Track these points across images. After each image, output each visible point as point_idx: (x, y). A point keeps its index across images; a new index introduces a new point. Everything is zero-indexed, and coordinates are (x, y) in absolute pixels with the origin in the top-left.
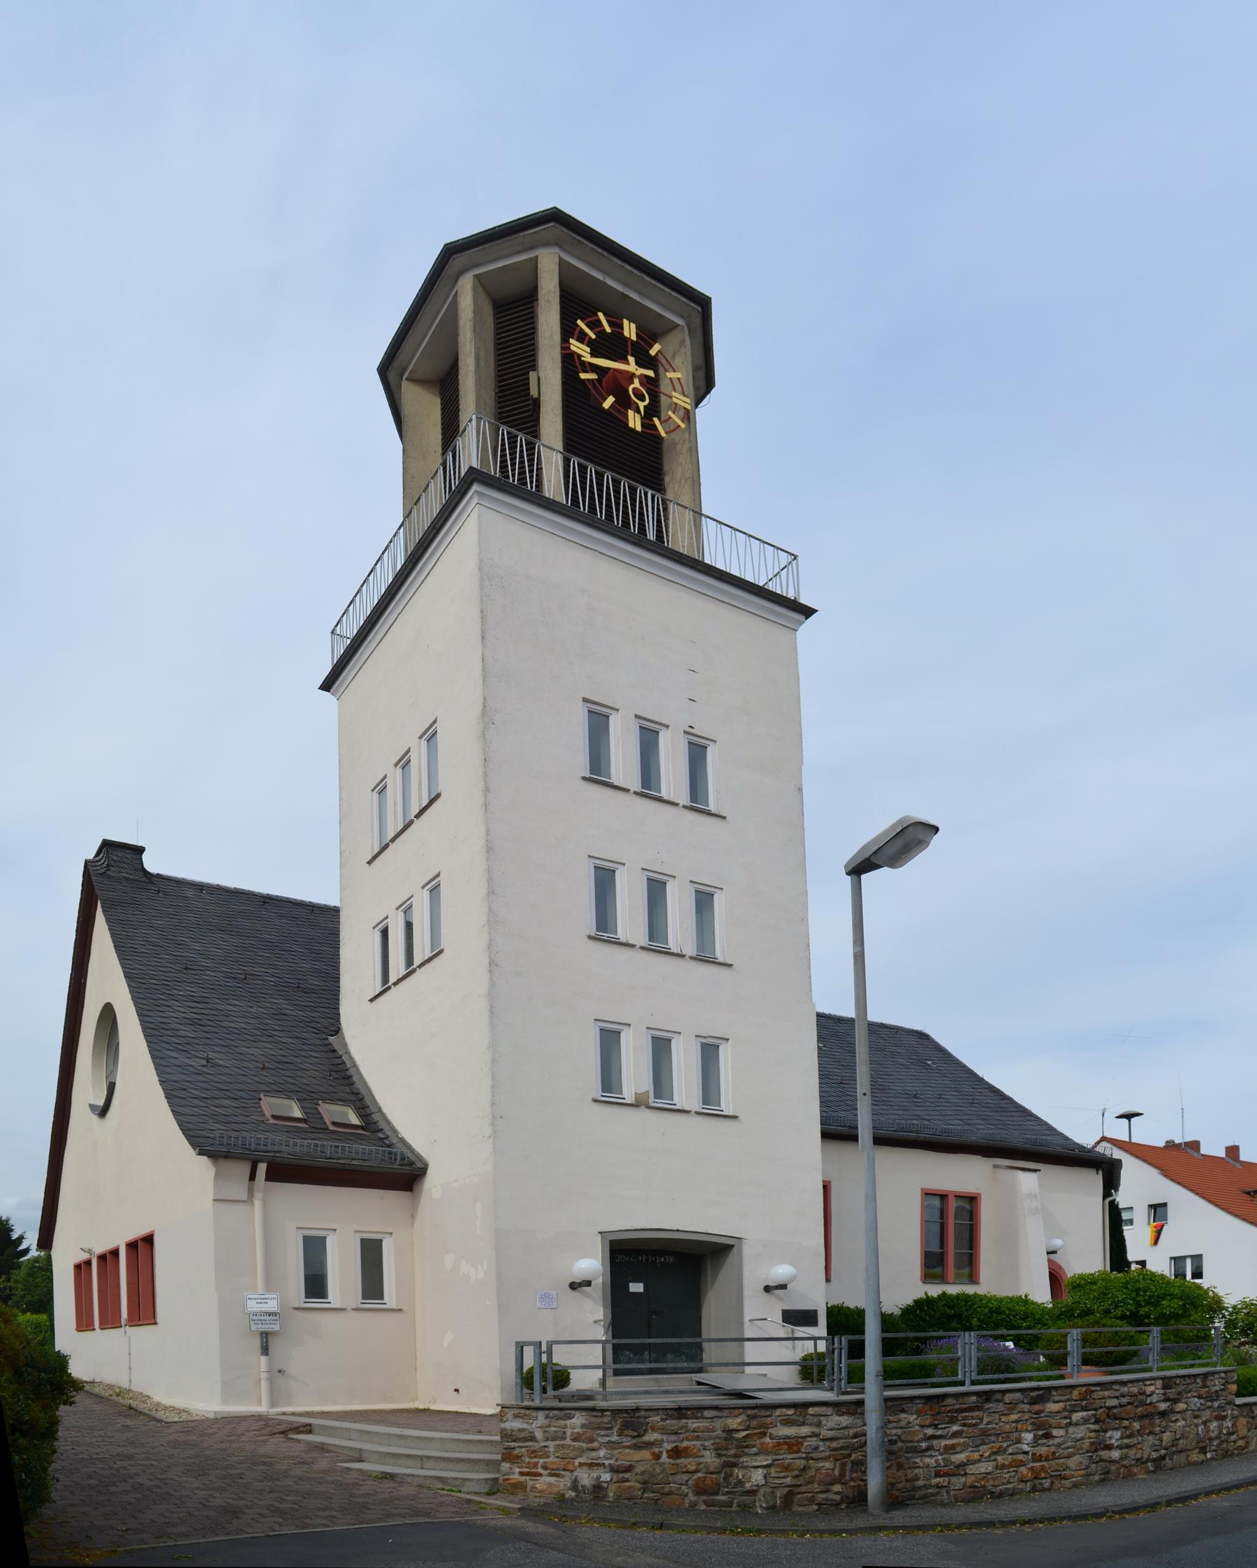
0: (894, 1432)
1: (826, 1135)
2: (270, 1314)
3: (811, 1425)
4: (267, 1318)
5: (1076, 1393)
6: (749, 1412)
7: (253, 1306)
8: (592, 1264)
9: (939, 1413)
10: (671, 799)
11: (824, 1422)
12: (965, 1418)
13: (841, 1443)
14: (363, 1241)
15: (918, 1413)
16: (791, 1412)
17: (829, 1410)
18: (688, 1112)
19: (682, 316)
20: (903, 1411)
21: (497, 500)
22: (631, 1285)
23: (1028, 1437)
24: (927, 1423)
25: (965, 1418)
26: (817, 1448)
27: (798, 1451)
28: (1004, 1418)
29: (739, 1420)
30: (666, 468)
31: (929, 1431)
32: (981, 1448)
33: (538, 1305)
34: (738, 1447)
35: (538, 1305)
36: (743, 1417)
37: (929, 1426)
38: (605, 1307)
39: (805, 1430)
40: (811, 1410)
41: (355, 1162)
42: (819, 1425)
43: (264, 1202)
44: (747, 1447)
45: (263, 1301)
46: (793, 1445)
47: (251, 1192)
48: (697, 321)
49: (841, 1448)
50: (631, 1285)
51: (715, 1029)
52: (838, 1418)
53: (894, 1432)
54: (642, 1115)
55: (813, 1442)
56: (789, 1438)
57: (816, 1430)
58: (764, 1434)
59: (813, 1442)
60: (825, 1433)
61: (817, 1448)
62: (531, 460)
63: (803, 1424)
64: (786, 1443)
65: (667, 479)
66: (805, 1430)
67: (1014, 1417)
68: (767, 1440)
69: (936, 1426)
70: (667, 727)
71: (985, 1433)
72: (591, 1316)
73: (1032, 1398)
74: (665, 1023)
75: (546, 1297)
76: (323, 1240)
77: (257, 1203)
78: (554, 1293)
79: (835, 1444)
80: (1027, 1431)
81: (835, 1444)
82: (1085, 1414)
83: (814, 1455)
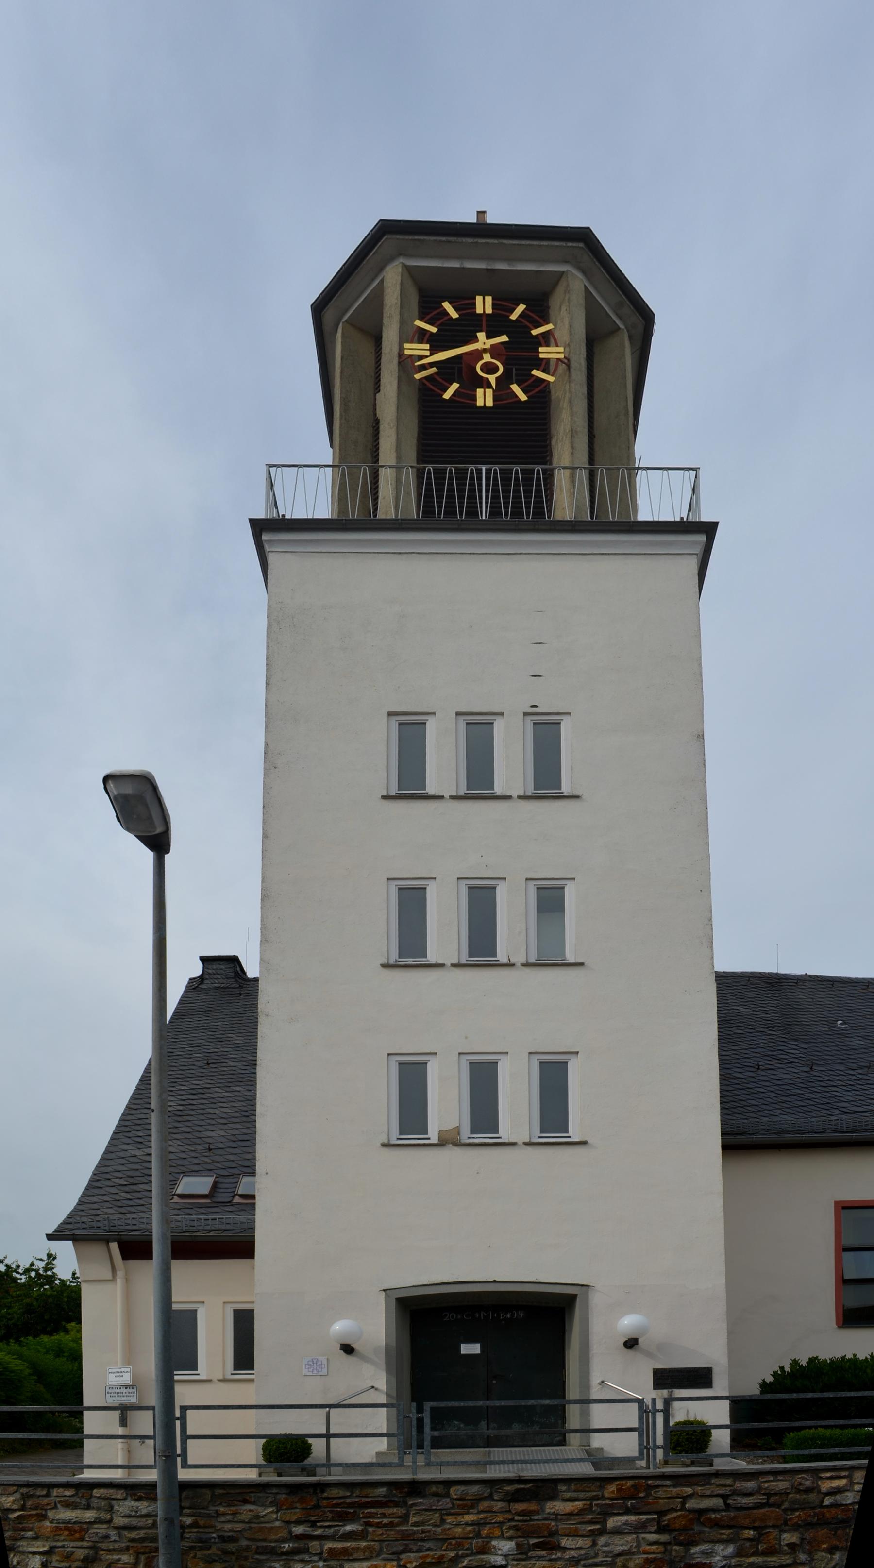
0: (228, 1526)
1: (728, 1148)
2: (126, 1387)
3: (98, 1509)
4: (124, 1390)
5: (612, 1488)
6: (24, 1490)
7: (113, 1380)
8: (375, 1327)
9: (317, 1507)
10: (504, 794)
11: (116, 1508)
12: (371, 1515)
13: (142, 1534)
14: (236, 1312)
15: (279, 1506)
16: (68, 1493)
17: (120, 1494)
18: (514, 1144)
19: (566, 262)
20: (246, 1502)
21: (569, 542)
22: (463, 1346)
23: (506, 1546)
24: (294, 1518)
25: (371, 1515)
26: (107, 1537)
27: (82, 1539)
28: (449, 1519)
29: (11, 1498)
30: (553, 431)
31: (298, 1530)
32: (403, 1556)
33: (305, 1372)
34: (15, 1529)
35: (305, 1372)
36: (18, 1495)
37: (298, 1522)
38: (388, 1371)
39: (90, 1515)
40: (96, 1492)
41: (211, 1234)
42: (111, 1509)
43: (127, 1280)
44: (24, 1529)
45: (120, 1375)
46: (76, 1530)
47: (114, 1269)
48: (587, 259)
49: (142, 1540)
50: (463, 1346)
51: (554, 1042)
52: (133, 1503)
53: (228, 1526)
54: (451, 1153)
55: (101, 1529)
56: (69, 1522)
57: (105, 1516)
58: (44, 1517)
59: (101, 1529)
60: (119, 1521)
61: (107, 1537)
62: (429, 496)
63: (88, 1507)
64: (66, 1528)
65: (553, 442)
66: (90, 1515)
67: (469, 1518)
68: (48, 1524)
69: (313, 1524)
70: (502, 714)
71: (406, 1536)
72: (374, 1379)
73: (507, 1493)
74: (482, 1045)
75: (314, 1363)
76: (194, 1312)
77: (119, 1281)
78: (323, 1359)
79: (133, 1535)
80: (502, 1537)
81: (133, 1535)
82: (632, 1518)
83: (104, 1546)
